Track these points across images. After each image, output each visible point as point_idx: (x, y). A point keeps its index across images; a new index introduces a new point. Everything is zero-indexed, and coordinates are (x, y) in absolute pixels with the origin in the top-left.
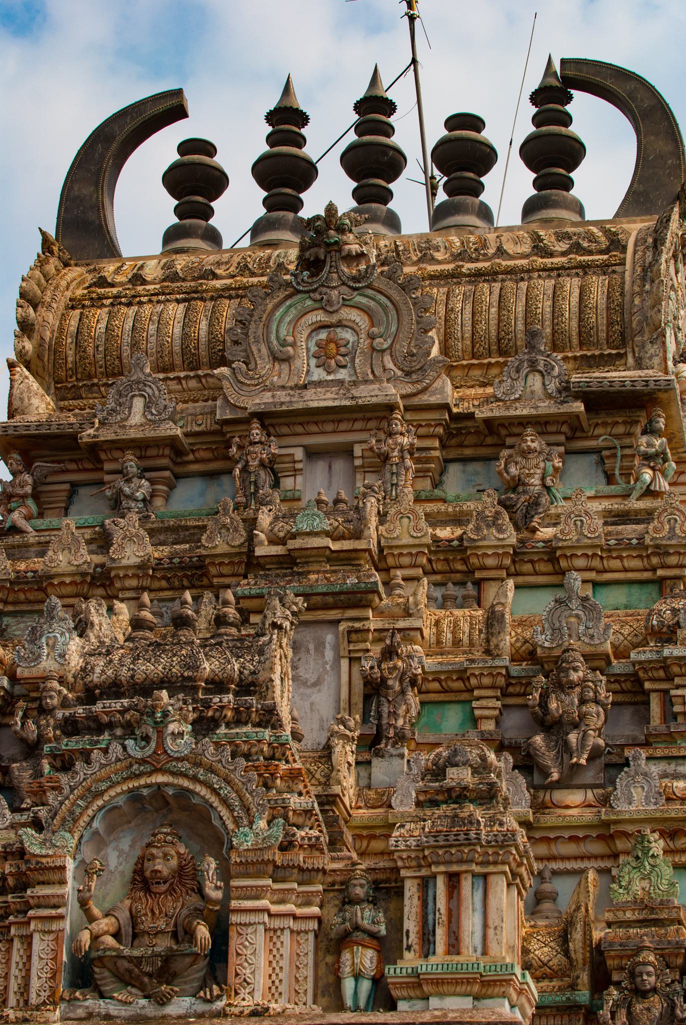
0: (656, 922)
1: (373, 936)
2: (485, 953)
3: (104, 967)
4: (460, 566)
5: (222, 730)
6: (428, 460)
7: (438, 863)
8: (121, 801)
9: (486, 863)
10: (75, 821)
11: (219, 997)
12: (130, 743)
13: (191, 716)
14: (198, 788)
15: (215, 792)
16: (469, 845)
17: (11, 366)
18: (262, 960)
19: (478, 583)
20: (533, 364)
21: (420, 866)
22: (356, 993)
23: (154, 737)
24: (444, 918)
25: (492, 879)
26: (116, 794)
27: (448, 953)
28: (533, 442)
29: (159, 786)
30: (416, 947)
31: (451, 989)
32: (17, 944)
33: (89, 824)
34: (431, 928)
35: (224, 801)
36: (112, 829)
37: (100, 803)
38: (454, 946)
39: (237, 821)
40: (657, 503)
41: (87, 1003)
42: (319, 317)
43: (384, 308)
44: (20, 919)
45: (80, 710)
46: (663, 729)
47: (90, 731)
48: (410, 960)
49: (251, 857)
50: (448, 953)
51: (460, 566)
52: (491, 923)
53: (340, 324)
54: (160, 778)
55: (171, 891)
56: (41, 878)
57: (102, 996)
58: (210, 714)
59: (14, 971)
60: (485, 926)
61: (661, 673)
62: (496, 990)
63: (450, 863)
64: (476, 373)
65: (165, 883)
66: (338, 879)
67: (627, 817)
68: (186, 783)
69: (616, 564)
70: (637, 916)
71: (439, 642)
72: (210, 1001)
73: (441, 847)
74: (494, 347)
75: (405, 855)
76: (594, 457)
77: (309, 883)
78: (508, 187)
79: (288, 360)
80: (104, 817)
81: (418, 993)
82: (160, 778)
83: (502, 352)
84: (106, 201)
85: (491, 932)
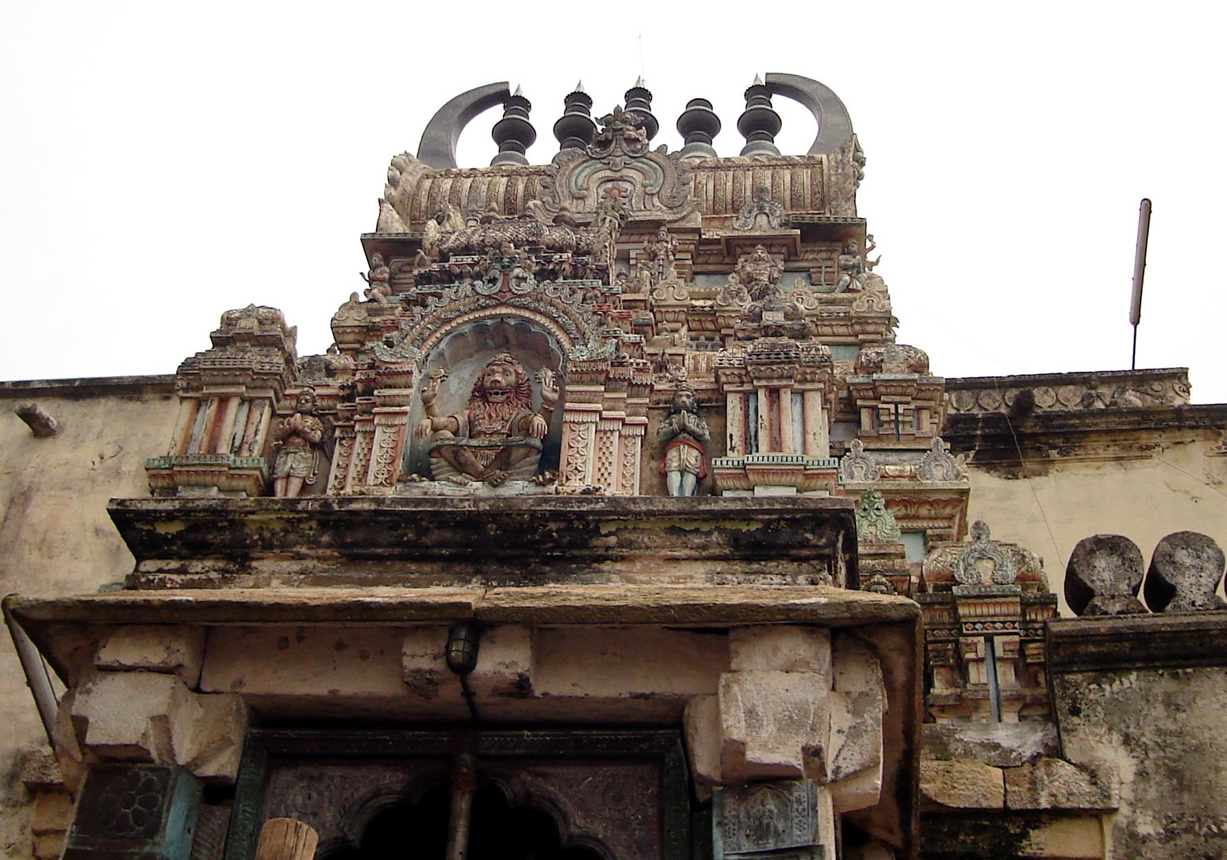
0: (883, 556)
1: (698, 438)
2: (805, 450)
3: (442, 456)
5: (561, 280)
6: (684, 266)
7: (759, 379)
8: (467, 329)
9: (804, 381)
10: (424, 341)
11: (551, 481)
12: (478, 283)
13: (535, 268)
15: (554, 320)
16: (789, 363)
17: (380, 201)
18: (591, 453)
20: (761, 209)
21: (742, 383)
24: (766, 423)
25: (808, 395)
26: (464, 324)
27: (772, 449)
28: (760, 252)
30: (740, 448)
31: (777, 479)
32: (359, 438)
33: (436, 345)
34: (753, 434)
35: (562, 328)
36: (457, 359)
37: (448, 328)
39: (573, 342)
41: (423, 484)
42: (608, 173)
43: (654, 169)
44: (366, 417)
45: (435, 266)
47: (441, 281)
50: (772, 449)
52: (809, 429)
53: (621, 179)
54: (504, 311)
55: (508, 401)
56: (389, 382)
58: (551, 267)
59: (354, 459)
60: (804, 432)
61: (871, 394)
62: (820, 482)
63: (771, 378)
64: (716, 223)
65: (503, 394)
66: (663, 398)
67: (722, 707)
68: (527, 314)
69: (827, 330)
71: (696, 369)
72: (542, 485)
73: (763, 365)
74: (729, 207)
75: (728, 372)
76: (804, 274)
77: (638, 396)
78: (728, 143)
79: (582, 198)
81: (743, 483)
82: (504, 311)
83: (736, 210)
84: (453, 138)
85: (810, 437)
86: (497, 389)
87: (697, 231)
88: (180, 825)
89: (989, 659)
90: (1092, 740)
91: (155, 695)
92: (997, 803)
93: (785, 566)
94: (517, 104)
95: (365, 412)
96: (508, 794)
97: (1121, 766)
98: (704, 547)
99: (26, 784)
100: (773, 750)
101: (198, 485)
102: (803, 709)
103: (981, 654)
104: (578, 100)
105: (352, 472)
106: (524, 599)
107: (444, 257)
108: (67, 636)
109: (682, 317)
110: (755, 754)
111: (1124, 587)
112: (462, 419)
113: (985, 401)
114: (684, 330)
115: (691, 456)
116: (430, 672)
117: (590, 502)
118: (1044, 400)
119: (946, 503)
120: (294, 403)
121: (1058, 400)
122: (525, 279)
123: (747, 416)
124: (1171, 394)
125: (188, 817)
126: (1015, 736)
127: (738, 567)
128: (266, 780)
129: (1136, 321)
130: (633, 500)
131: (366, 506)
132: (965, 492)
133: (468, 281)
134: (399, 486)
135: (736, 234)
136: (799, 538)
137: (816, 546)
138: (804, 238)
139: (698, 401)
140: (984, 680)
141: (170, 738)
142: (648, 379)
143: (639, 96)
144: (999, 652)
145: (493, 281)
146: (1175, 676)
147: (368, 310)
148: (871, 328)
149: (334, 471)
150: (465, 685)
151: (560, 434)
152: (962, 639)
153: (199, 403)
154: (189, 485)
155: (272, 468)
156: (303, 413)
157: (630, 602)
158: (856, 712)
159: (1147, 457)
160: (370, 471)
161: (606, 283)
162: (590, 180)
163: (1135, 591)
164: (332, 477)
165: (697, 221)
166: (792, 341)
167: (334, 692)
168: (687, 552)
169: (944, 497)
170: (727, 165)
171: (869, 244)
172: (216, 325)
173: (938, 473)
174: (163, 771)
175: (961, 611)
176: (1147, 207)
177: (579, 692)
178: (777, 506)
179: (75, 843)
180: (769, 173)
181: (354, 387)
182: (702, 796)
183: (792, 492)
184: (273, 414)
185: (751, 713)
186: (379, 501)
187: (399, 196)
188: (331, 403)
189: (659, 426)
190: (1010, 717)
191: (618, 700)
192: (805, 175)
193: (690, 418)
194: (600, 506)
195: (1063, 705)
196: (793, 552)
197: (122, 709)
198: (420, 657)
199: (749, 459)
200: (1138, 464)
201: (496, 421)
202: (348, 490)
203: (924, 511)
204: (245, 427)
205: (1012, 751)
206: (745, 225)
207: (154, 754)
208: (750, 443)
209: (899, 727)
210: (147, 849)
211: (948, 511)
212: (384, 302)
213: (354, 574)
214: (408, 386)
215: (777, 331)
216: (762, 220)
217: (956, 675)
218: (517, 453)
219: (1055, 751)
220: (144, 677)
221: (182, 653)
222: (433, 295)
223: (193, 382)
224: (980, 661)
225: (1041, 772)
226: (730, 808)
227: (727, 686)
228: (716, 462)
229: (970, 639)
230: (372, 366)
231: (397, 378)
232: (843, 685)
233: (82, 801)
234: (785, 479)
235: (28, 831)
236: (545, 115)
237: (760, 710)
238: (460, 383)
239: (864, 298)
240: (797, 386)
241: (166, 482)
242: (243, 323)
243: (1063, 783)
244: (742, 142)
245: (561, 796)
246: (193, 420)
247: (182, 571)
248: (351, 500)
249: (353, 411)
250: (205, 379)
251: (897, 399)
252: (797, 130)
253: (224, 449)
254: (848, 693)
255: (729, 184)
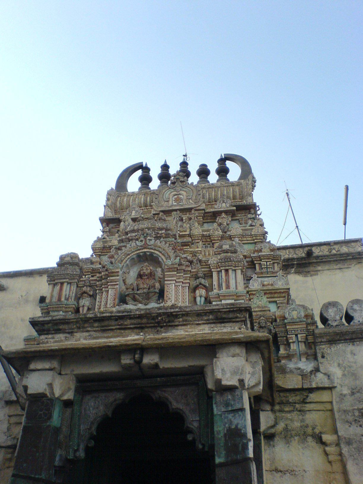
1: (205, 286)
2: (236, 289)
4: (209, 240)
5: (162, 239)
7: (222, 267)
8: (135, 256)
9: (236, 267)
10: (122, 261)
11: (162, 302)
12: (137, 242)
14: (156, 252)
15: (161, 252)
17: (105, 206)
19: (213, 244)
21: (217, 268)
22: (200, 301)
23: (144, 240)
26: (133, 255)
28: (223, 215)
29: (145, 252)
31: (228, 297)
32: (104, 293)
33: (126, 262)
35: (163, 254)
38: (228, 287)
40: (254, 227)
44: (106, 286)
45: (124, 237)
46: (260, 271)
48: (216, 291)
49: (171, 266)
51: (209, 240)
54: (145, 250)
55: (148, 278)
56: (112, 275)
57: (127, 304)
59: (103, 300)
60: (236, 283)
64: (210, 206)
67: (214, 369)
68: (152, 251)
69: (245, 239)
70: (259, 310)
72: (160, 304)
78: (213, 178)
80: (130, 261)
82: (145, 250)
85: (238, 284)
86: (144, 275)
87: (204, 210)
88: (57, 416)
89: (297, 342)
90: (328, 366)
91: (48, 377)
92: (300, 387)
93: (230, 324)
94: (146, 169)
95: (105, 285)
96: (154, 397)
97: (337, 372)
98: (208, 320)
99: (5, 401)
100: (229, 381)
101: (56, 311)
102: (237, 368)
103: (294, 340)
104: (165, 167)
105: (103, 303)
106: (156, 340)
107: (127, 233)
108: (20, 362)
109: (200, 238)
110: (224, 383)
111: (338, 318)
112: (135, 285)
113: (297, 252)
114: (201, 243)
115: (203, 292)
116: (130, 364)
117: (174, 309)
118: (316, 251)
119: (283, 293)
120: (83, 283)
121: (321, 251)
122: (151, 240)
123: (219, 278)
124: (357, 246)
125: (59, 412)
126: (306, 366)
127: (219, 325)
128: (82, 399)
129: (345, 224)
130: (186, 307)
131: (108, 315)
132: (289, 289)
133: (134, 241)
134: (117, 307)
135: (216, 210)
136: (235, 316)
137: (240, 318)
138: (237, 210)
139: (204, 274)
140: (295, 348)
141: (53, 390)
142: (190, 269)
143: (184, 164)
144: (300, 340)
145: (142, 241)
146: (353, 345)
147: (103, 242)
148: (259, 238)
149: (97, 303)
150: (140, 367)
151: (164, 287)
152: (288, 336)
153: (55, 285)
154: (53, 311)
155: (78, 303)
156: (86, 286)
157: (187, 340)
158: (253, 367)
159: (350, 268)
160: (107, 302)
161: (176, 239)
162: (169, 194)
163: (341, 318)
164: (97, 305)
165: (203, 206)
166: (231, 254)
167: (101, 371)
168: (203, 322)
169: (282, 291)
170: (213, 186)
171: (258, 209)
172: (58, 260)
173: (280, 283)
174: (51, 400)
175: (288, 327)
176: (347, 188)
177: (173, 366)
178: (228, 307)
179: (26, 423)
180: (225, 189)
181: (101, 277)
182: (210, 395)
183: (233, 301)
184: (77, 286)
185: (223, 370)
186: (111, 312)
187: (110, 205)
188: (95, 282)
189: (194, 283)
190: (303, 359)
191: (184, 368)
192: (237, 189)
193: (201, 278)
194: (177, 310)
195: (319, 355)
196: (234, 320)
197: (37, 382)
198: (126, 360)
199: (220, 292)
200: (346, 270)
201: (144, 285)
202: (102, 309)
203: (276, 295)
204: (69, 290)
205: (304, 370)
206: (219, 206)
207: (48, 394)
208: (220, 287)
209: (267, 369)
210: (48, 424)
211: (284, 295)
212: (108, 239)
213: (106, 335)
214: (118, 276)
215: (226, 252)
216: (224, 205)
217: (287, 347)
218: (151, 295)
219: (317, 370)
220: (44, 372)
221: (55, 364)
222: (124, 246)
223: (52, 276)
224: (293, 342)
225: (313, 376)
226: (218, 398)
227: (216, 362)
228: (210, 293)
229: (291, 336)
230: (107, 270)
231: (115, 274)
232: (249, 360)
233: (27, 411)
234: (230, 298)
235: (6, 416)
236: (155, 172)
237: (225, 369)
238: (133, 273)
239: (256, 228)
240: (233, 268)
241: (46, 311)
242: (66, 259)
243: (320, 380)
244: (217, 177)
245: (169, 397)
246: (53, 291)
247: (53, 338)
248: (103, 313)
249: (102, 284)
250: (56, 278)
251: (267, 260)
252: (234, 172)
253: (63, 299)
254: (251, 362)
255: (213, 193)
